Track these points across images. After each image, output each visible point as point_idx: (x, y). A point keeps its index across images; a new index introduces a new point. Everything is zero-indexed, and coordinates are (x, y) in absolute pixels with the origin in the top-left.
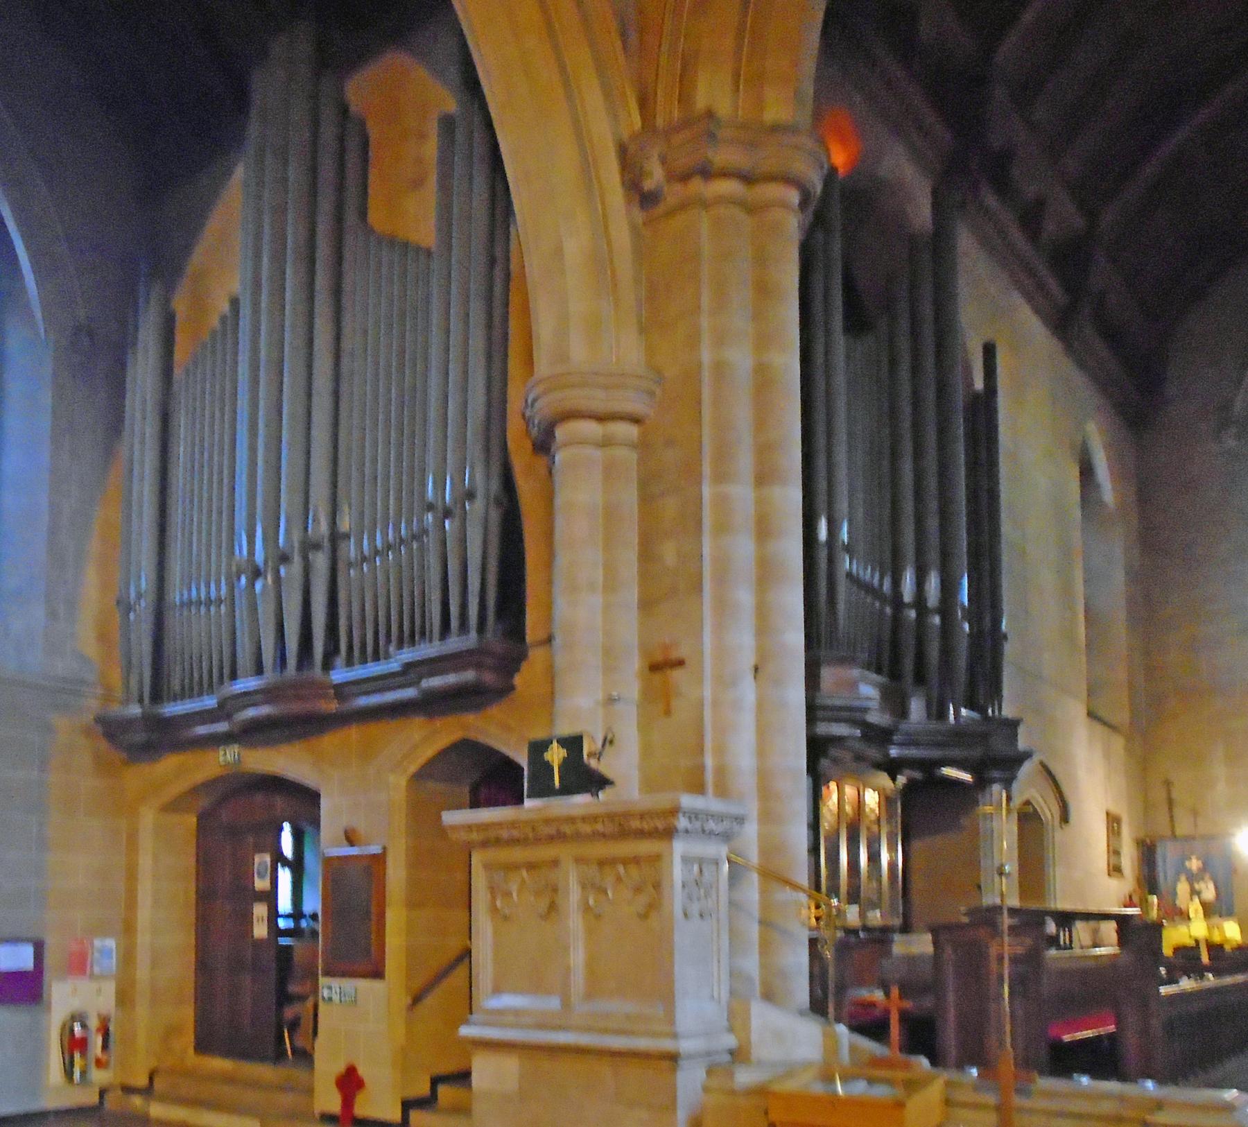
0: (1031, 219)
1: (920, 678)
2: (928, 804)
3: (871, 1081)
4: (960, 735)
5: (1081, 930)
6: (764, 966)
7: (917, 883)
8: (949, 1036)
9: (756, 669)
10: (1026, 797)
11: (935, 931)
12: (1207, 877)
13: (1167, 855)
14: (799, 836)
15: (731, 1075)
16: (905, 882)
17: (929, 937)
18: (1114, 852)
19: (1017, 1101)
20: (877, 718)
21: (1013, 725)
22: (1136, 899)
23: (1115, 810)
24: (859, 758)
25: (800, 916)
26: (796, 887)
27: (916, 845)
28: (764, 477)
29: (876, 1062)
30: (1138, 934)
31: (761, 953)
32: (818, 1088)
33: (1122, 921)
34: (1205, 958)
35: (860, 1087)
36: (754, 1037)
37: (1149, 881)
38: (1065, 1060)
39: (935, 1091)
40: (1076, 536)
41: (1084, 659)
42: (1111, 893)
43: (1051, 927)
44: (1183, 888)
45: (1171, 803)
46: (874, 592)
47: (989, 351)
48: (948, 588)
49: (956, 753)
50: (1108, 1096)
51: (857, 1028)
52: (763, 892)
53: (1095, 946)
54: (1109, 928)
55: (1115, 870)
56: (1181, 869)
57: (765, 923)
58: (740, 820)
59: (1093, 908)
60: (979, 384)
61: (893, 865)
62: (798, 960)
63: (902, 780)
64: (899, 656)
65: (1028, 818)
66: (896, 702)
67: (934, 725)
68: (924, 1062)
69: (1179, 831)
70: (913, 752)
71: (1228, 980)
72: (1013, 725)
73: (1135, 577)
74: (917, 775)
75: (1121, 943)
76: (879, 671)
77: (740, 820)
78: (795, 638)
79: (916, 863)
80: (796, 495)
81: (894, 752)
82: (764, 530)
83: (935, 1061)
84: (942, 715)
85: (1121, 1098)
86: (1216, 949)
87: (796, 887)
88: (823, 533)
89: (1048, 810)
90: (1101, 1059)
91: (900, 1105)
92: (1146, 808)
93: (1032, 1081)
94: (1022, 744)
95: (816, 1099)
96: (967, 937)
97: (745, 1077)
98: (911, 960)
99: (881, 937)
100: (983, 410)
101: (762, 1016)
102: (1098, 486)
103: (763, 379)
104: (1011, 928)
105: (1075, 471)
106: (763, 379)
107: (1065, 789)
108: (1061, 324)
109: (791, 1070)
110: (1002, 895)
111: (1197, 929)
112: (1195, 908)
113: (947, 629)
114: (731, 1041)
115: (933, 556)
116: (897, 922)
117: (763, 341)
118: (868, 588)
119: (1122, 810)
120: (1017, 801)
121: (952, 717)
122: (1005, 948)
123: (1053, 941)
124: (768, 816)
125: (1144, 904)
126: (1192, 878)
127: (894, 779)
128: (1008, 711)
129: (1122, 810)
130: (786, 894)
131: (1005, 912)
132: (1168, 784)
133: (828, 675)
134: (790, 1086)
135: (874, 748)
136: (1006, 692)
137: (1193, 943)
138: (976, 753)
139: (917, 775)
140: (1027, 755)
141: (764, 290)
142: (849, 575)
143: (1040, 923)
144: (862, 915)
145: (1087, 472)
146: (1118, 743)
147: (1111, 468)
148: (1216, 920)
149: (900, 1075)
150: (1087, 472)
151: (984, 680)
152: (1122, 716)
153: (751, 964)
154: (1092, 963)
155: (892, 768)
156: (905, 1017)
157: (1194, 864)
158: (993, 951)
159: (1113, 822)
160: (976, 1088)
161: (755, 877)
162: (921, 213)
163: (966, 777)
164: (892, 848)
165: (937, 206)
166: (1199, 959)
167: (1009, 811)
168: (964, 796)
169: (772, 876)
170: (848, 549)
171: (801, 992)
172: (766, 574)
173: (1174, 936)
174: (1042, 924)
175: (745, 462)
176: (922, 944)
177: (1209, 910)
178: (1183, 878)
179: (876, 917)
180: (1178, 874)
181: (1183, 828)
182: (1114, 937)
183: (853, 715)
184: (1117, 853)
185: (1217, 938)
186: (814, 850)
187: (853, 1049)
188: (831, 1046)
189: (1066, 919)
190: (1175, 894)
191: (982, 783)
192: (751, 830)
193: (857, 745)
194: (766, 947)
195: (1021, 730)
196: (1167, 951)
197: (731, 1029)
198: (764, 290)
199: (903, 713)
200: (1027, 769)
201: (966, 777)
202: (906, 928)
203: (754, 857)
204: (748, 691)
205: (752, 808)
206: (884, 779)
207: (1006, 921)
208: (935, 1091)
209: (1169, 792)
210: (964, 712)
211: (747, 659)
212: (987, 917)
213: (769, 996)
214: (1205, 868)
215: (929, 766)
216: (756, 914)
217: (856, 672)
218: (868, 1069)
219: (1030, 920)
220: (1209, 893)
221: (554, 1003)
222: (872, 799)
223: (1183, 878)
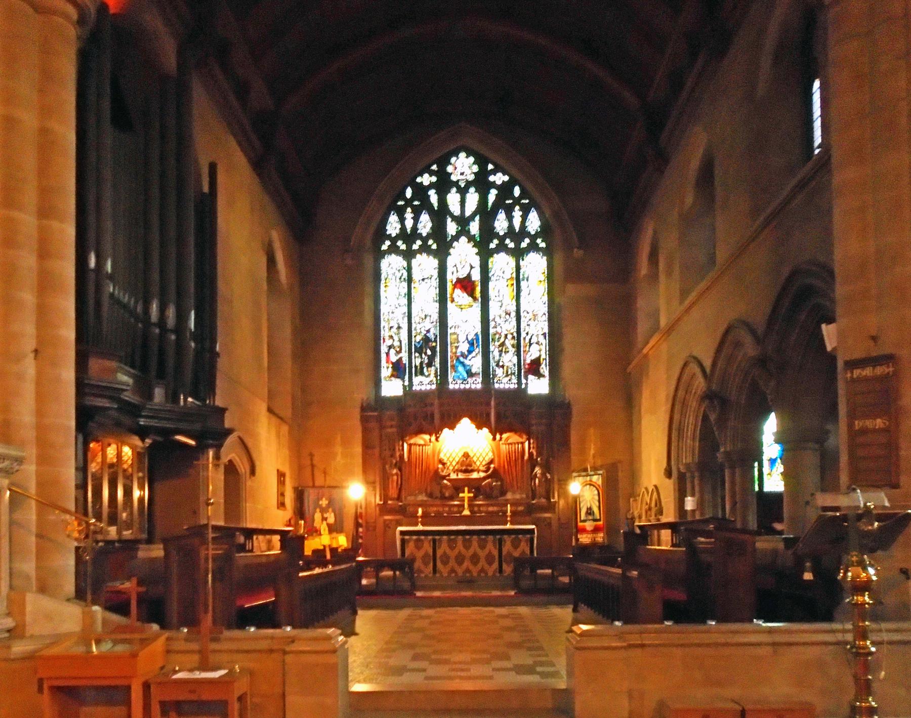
0: (242, 90)
1: (161, 375)
2: (165, 461)
3: (116, 642)
4: (187, 415)
5: (259, 542)
6: (38, 568)
7: (157, 509)
8: (173, 608)
9: (36, 351)
10: (229, 458)
11: (165, 541)
12: (330, 510)
13: (310, 496)
14: (69, 474)
15: (9, 647)
16: (150, 510)
17: (161, 546)
18: (282, 494)
19: (214, 646)
20: (128, 396)
21: (222, 411)
22: (292, 522)
23: (282, 469)
24: (118, 424)
25: (70, 533)
26: (67, 511)
27: (157, 486)
28: (45, 211)
29: (120, 629)
30: (292, 542)
31: (37, 558)
32: (80, 650)
33: (283, 534)
34: (328, 557)
35: (107, 646)
36: (28, 619)
37: (300, 512)
38: (244, 618)
39: (159, 644)
40: (264, 301)
41: (266, 375)
42: (279, 519)
43: (241, 539)
44: (318, 516)
45: (313, 466)
46: (132, 313)
47: (213, 168)
48: (181, 317)
49: (182, 426)
50: (266, 638)
51: (111, 607)
52: (40, 515)
53: (269, 550)
54: (276, 538)
55: (281, 505)
56: (317, 505)
57: (39, 536)
58: (20, 460)
59: (267, 527)
60: (206, 189)
61: (141, 500)
62: (66, 564)
63: (148, 441)
64: (150, 356)
65: (231, 469)
66: (144, 389)
67: (169, 406)
68: (155, 627)
69: (317, 483)
70: (153, 423)
71: (337, 568)
72: (222, 411)
73: (296, 332)
74: (159, 439)
75: (282, 548)
76: (133, 367)
77: (20, 460)
78: (69, 333)
79: (157, 499)
80: (71, 231)
81: (142, 422)
82: (44, 252)
83: (163, 626)
84: (176, 400)
85: (272, 638)
86: (334, 550)
87: (67, 511)
88: (92, 263)
89: (243, 467)
90: (265, 617)
91: (134, 656)
92: (299, 470)
93: (221, 633)
94: (227, 425)
95: (72, 658)
96: (186, 544)
97: (19, 648)
98: (153, 560)
99: (130, 546)
100: (206, 209)
101: (34, 602)
102: (277, 272)
103: (46, 142)
104: (213, 538)
105: (264, 260)
106: (46, 142)
107: (254, 456)
108: (258, 165)
109: (58, 639)
110: (208, 518)
111: (324, 540)
112: (324, 528)
113: (180, 345)
114: (9, 623)
115: (172, 295)
116: (145, 536)
117: (46, 111)
118: (125, 307)
119: (286, 469)
120: (225, 460)
121: (182, 403)
122: (211, 551)
123: (242, 548)
124: (43, 459)
125: (297, 525)
126: (323, 511)
127: (143, 440)
128: (219, 402)
129: (286, 469)
130: (54, 516)
131: (210, 530)
132: (311, 455)
133: (95, 365)
134: (55, 651)
135: (128, 421)
136: (218, 391)
137: (322, 548)
138: (197, 427)
139: (159, 439)
140: (229, 432)
141: (47, 76)
142: (112, 295)
143: (236, 536)
144: (119, 532)
145: (271, 261)
146: (285, 429)
147: (286, 264)
148: (334, 535)
149: (137, 636)
150: (271, 261)
151: (204, 379)
152: (287, 413)
153: (29, 567)
154: (264, 560)
155: (142, 433)
156: (141, 600)
157: (324, 502)
158: (203, 553)
159: (281, 475)
160: (186, 640)
161: (33, 503)
162: (170, 61)
163: (192, 442)
164: (142, 488)
165: (180, 53)
166: (325, 557)
167: (216, 466)
168: (191, 455)
169: (48, 503)
170: (111, 277)
171: (69, 586)
172: (45, 284)
173: (311, 545)
174: (233, 536)
175: (30, 197)
176: (157, 551)
177: (332, 529)
178: (318, 510)
179: (127, 534)
180: (315, 509)
181: (319, 481)
182: (279, 544)
183: (113, 393)
184: (283, 495)
185: (335, 545)
186: (82, 486)
187: (105, 622)
188: (88, 618)
189: (250, 533)
190: (313, 520)
191: (201, 448)
192: (31, 468)
193: (114, 414)
194: (41, 554)
195: (227, 414)
196: (308, 552)
197: (9, 614)
198: (47, 76)
199: (150, 396)
200: (231, 440)
201: (192, 442)
202: (150, 541)
203: (33, 489)
204: (29, 367)
205: (31, 452)
206: (136, 441)
207: (211, 535)
208: (159, 644)
209: (312, 460)
210: (190, 399)
211: (30, 344)
212: (199, 531)
213: (43, 589)
214: (329, 505)
215: (168, 433)
216: (34, 529)
217: (114, 364)
218: (112, 631)
219: (226, 534)
220: (331, 520)
221: (583, 517)
222: (127, 451)
223: (318, 510)
